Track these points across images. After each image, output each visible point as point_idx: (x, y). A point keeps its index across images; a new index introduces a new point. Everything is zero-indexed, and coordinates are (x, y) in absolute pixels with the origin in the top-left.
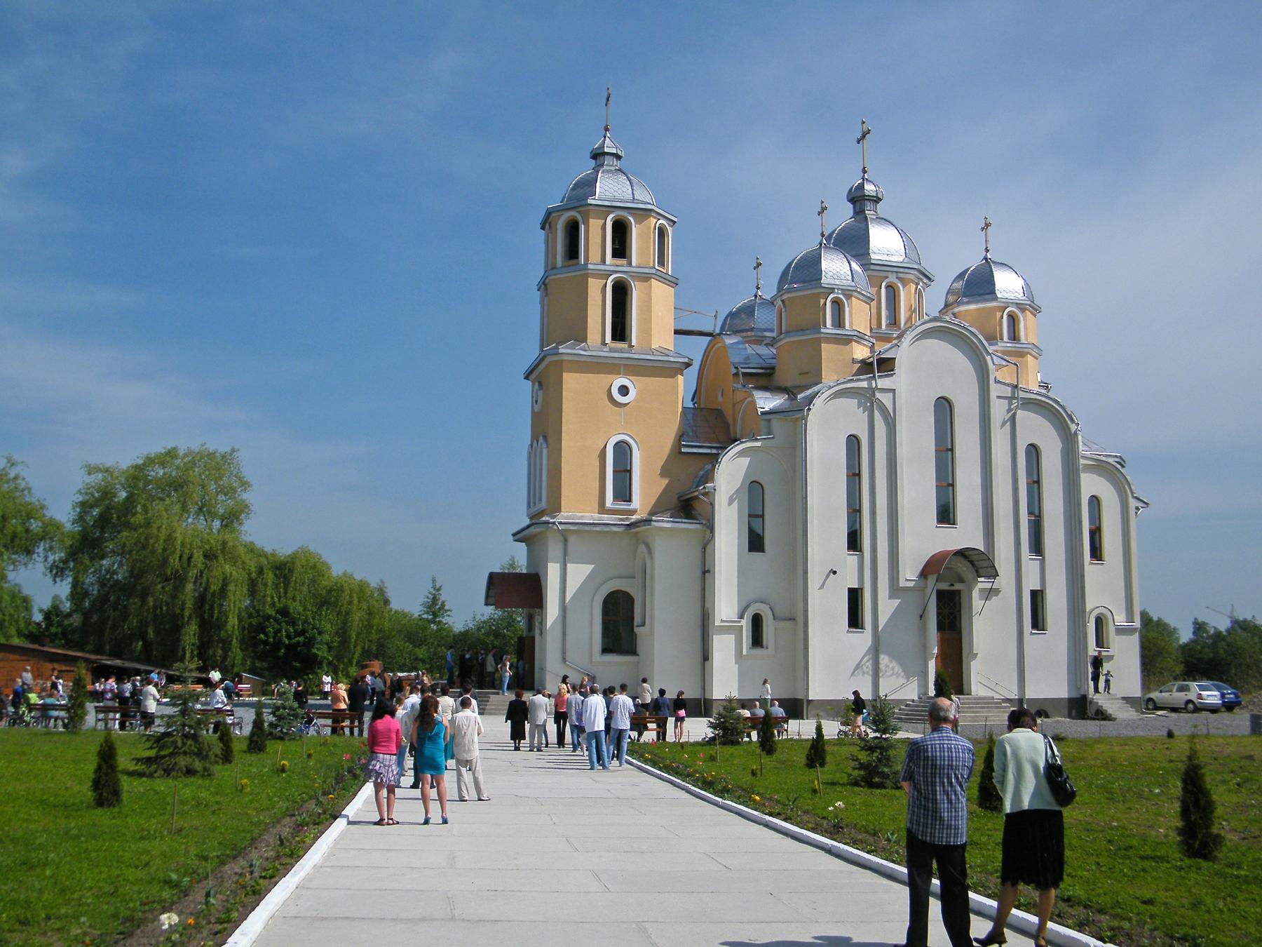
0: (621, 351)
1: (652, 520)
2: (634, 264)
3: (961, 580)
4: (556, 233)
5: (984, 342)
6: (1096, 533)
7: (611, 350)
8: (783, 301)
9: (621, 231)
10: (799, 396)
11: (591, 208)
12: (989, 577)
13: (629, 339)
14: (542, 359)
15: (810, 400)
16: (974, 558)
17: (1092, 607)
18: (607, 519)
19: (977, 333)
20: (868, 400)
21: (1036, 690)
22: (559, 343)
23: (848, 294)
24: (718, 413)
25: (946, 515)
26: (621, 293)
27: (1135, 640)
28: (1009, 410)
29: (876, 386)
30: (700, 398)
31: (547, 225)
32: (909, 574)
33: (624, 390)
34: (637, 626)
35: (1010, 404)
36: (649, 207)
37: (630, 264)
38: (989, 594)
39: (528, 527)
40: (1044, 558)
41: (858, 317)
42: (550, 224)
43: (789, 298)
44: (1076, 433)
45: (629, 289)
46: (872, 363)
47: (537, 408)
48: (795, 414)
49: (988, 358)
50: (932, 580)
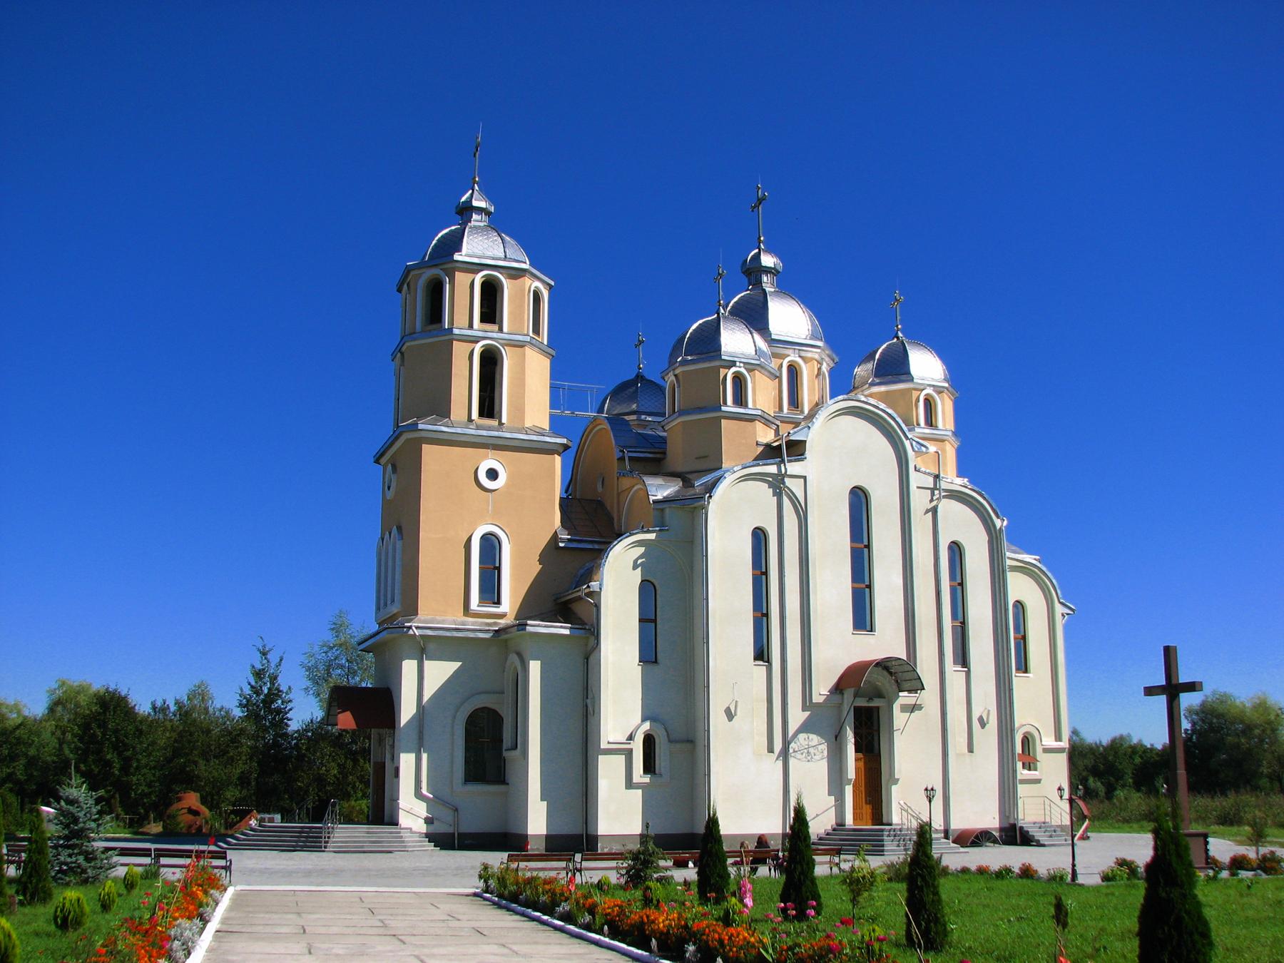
0: (489, 428)
2: (505, 329)
3: (880, 695)
5: (903, 426)
6: (1023, 640)
7: (478, 428)
8: (676, 376)
9: (491, 292)
10: (697, 484)
11: (457, 265)
14: (397, 438)
15: (710, 488)
18: (471, 623)
19: (895, 415)
20: (778, 485)
22: (419, 418)
23: (751, 368)
24: (599, 505)
25: (863, 618)
26: (491, 361)
27: (1063, 759)
28: (932, 500)
29: (786, 472)
30: (575, 487)
31: (405, 286)
32: (822, 689)
34: (506, 750)
35: (933, 494)
37: (501, 330)
38: (913, 708)
39: (378, 633)
40: (969, 670)
41: (762, 395)
42: (408, 285)
43: (683, 372)
45: (499, 357)
46: (780, 447)
47: (390, 495)
49: (907, 443)
50: (849, 694)
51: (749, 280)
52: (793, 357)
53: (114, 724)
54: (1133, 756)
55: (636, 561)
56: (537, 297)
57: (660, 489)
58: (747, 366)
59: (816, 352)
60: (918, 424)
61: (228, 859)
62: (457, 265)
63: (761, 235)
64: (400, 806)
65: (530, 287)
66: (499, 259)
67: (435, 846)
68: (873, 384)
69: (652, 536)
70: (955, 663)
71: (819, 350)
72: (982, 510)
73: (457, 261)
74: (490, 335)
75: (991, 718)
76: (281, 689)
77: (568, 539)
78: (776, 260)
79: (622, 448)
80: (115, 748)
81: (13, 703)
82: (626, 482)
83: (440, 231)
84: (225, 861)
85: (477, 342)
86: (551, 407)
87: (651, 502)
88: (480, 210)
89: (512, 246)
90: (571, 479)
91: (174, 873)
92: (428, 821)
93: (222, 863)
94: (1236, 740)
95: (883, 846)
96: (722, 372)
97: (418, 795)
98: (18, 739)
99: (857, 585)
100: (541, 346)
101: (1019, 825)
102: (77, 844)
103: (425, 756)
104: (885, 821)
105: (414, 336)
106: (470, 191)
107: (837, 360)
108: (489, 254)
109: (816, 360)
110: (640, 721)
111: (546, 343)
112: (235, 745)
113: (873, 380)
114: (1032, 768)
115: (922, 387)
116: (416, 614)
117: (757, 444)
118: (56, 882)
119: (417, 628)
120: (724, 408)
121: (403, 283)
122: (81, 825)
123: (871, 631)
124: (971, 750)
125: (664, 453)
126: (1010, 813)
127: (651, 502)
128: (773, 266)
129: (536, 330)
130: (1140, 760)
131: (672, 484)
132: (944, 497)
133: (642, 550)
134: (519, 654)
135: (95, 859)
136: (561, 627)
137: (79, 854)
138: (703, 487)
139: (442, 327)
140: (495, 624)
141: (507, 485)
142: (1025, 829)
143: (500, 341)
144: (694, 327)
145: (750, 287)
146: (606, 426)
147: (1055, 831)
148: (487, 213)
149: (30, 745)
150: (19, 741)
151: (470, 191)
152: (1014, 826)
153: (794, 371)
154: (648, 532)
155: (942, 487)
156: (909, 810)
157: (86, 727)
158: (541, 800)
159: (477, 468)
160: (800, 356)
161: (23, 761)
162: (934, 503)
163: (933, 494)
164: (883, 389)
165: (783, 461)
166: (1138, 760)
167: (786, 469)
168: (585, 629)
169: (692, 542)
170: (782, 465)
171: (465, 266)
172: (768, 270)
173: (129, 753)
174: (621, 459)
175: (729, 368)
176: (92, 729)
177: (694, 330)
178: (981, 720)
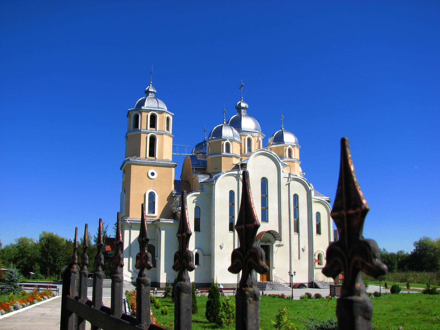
0: (152, 160)
1: (160, 220)
2: (158, 129)
4: (131, 118)
8: (209, 143)
9: (153, 118)
10: (214, 177)
12: (279, 240)
13: (155, 156)
15: (216, 178)
16: (274, 234)
17: (317, 251)
21: (296, 280)
22: (131, 157)
23: (231, 141)
26: (153, 140)
28: (288, 181)
31: (128, 116)
33: (153, 174)
35: (288, 179)
36: (163, 110)
37: (156, 130)
40: (299, 234)
41: (235, 149)
43: (211, 142)
44: (311, 190)
45: (155, 138)
48: (211, 184)
49: (280, 164)
51: (238, 111)
52: (249, 136)
53: (51, 247)
54: (398, 258)
55: (194, 201)
56: (168, 119)
57: (202, 178)
58: (230, 140)
59: (257, 134)
60: (286, 157)
61: (57, 288)
62: (143, 110)
63: (242, 96)
64: (123, 274)
65: (165, 116)
66: (156, 108)
67: (134, 286)
68: (273, 144)
69: (199, 193)
70: (294, 232)
71: (257, 134)
72: (303, 182)
73: (143, 109)
74: (152, 131)
75: (306, 248)
76: (107, 236)
77: (176, 194)
78: (246, 105)
79: (193, 165)
80: (52, 255)
81: (30, 238)
82: (194, 175)
83: (138, 100)
84: (56, 289)
85: (148, 134)
86: (173, 152)
87: (199, 182)
88: (152, 92)
89: (161, 103)
90: (181, 174)
91: (29, 291)
92: (132, 278)
93: (55, 289)
94: (430, 253)
95: (266, 286)
96: (222, 142)
97: (129, 270)
98: (25, 251)
99: (263, 208)
100: (170, 135)
101: (314, 282)
102: (12, 284)
103: (131, 259)
104: (270, 280)
105: (130, 132)
106: (149, 86)
107: (265, 136)
108: (153, 106)
109: (257, 137)
110: (194, 249)
111: (171, 133)
112: (92, 253)
113: (273, 143)
114: (321, 264)
115: (288, 145)
116: (129, 216)
117: (233, 164)
118: (6, 293)
119: (128, 221)
120: (222, 154)
121: (128, 115)
122: (13, 278)
123: (267, 222)
124: (299, 259)
125: (206, 167)
126: (311, 278)
127: (199, 182)
128: (245, 107)
129: (168, 129)
130: (400, 259)
131: (207, 177)
132: (292, 180)
133: (196, 197)
134: (159, 229)
135: (17, 287)
136: (171, 221)
137: (13, 286)
138: (215, 178)
139: (138, 129)
140: (153, 219)
141: (157, 177)
142: (316, 283)
143: (156, 133)
144: (215, 128)
145: (238, 113)
146: (189, 158)
147: (325, 284)
148: (154, 93)
149: (28, 253)
150: (25, 252)
151: (149, 86)
152: (313, 282)
153: (249, 140)
154: (198, 192)
155: (291, 177)
156: (275, 278)
157: (43, 247)
158: (165, 272)
159: (148, 172)
160: (251, 135)
161: (26, 258)
162: (289, 182)
163: (288, 179)
164: (275, 146)
165: (239, 170)
166: (400, 260)
167: (240, 173)
168: (178, 221)
169: (211, 195)
170: (239, 171)
171: (146, 110)
172: (243, 108)
173: (56, 256)
174: (193, 169)
175: (225, 141)
176: (44, 249)
177: (215, 129)
178: (303, 249)
